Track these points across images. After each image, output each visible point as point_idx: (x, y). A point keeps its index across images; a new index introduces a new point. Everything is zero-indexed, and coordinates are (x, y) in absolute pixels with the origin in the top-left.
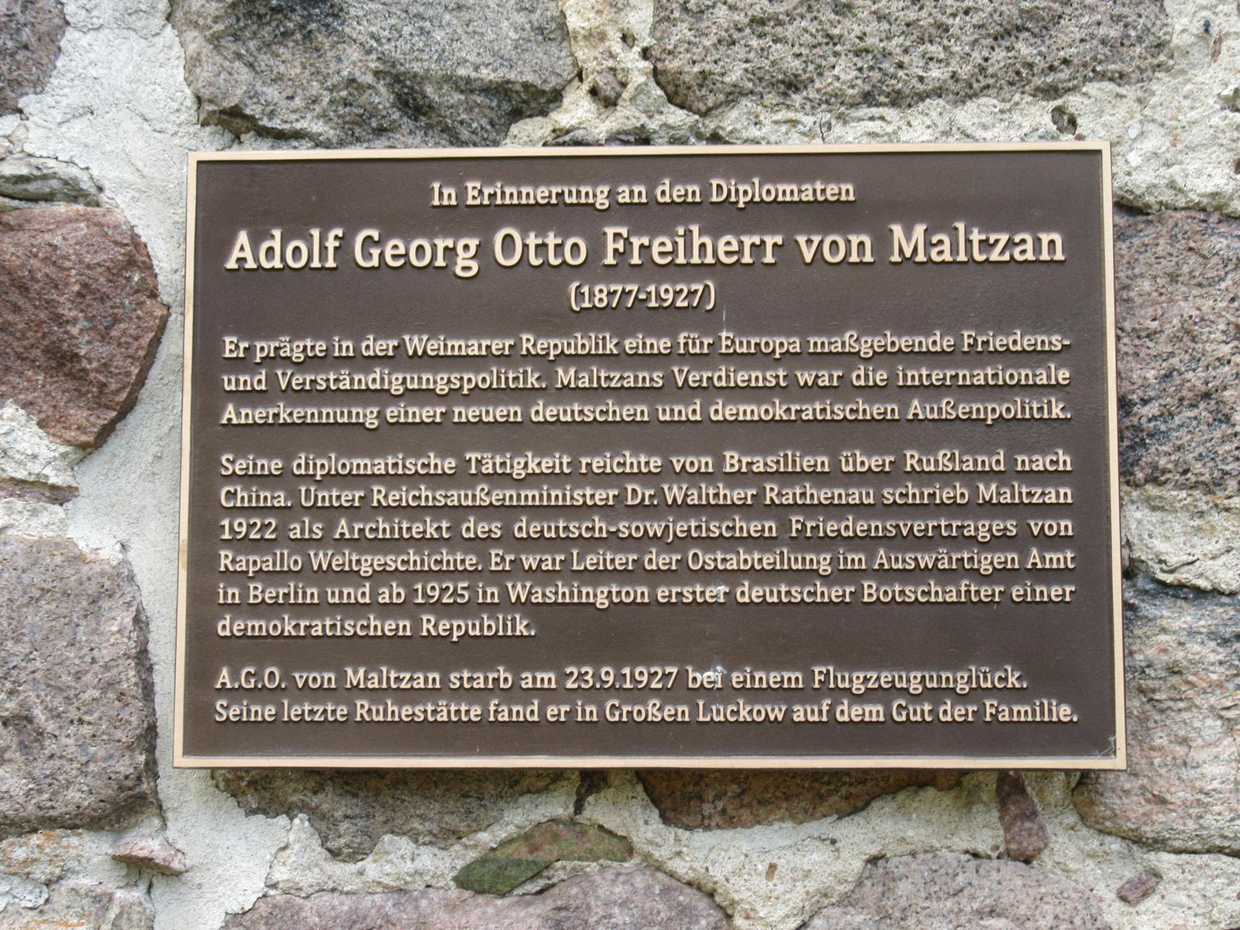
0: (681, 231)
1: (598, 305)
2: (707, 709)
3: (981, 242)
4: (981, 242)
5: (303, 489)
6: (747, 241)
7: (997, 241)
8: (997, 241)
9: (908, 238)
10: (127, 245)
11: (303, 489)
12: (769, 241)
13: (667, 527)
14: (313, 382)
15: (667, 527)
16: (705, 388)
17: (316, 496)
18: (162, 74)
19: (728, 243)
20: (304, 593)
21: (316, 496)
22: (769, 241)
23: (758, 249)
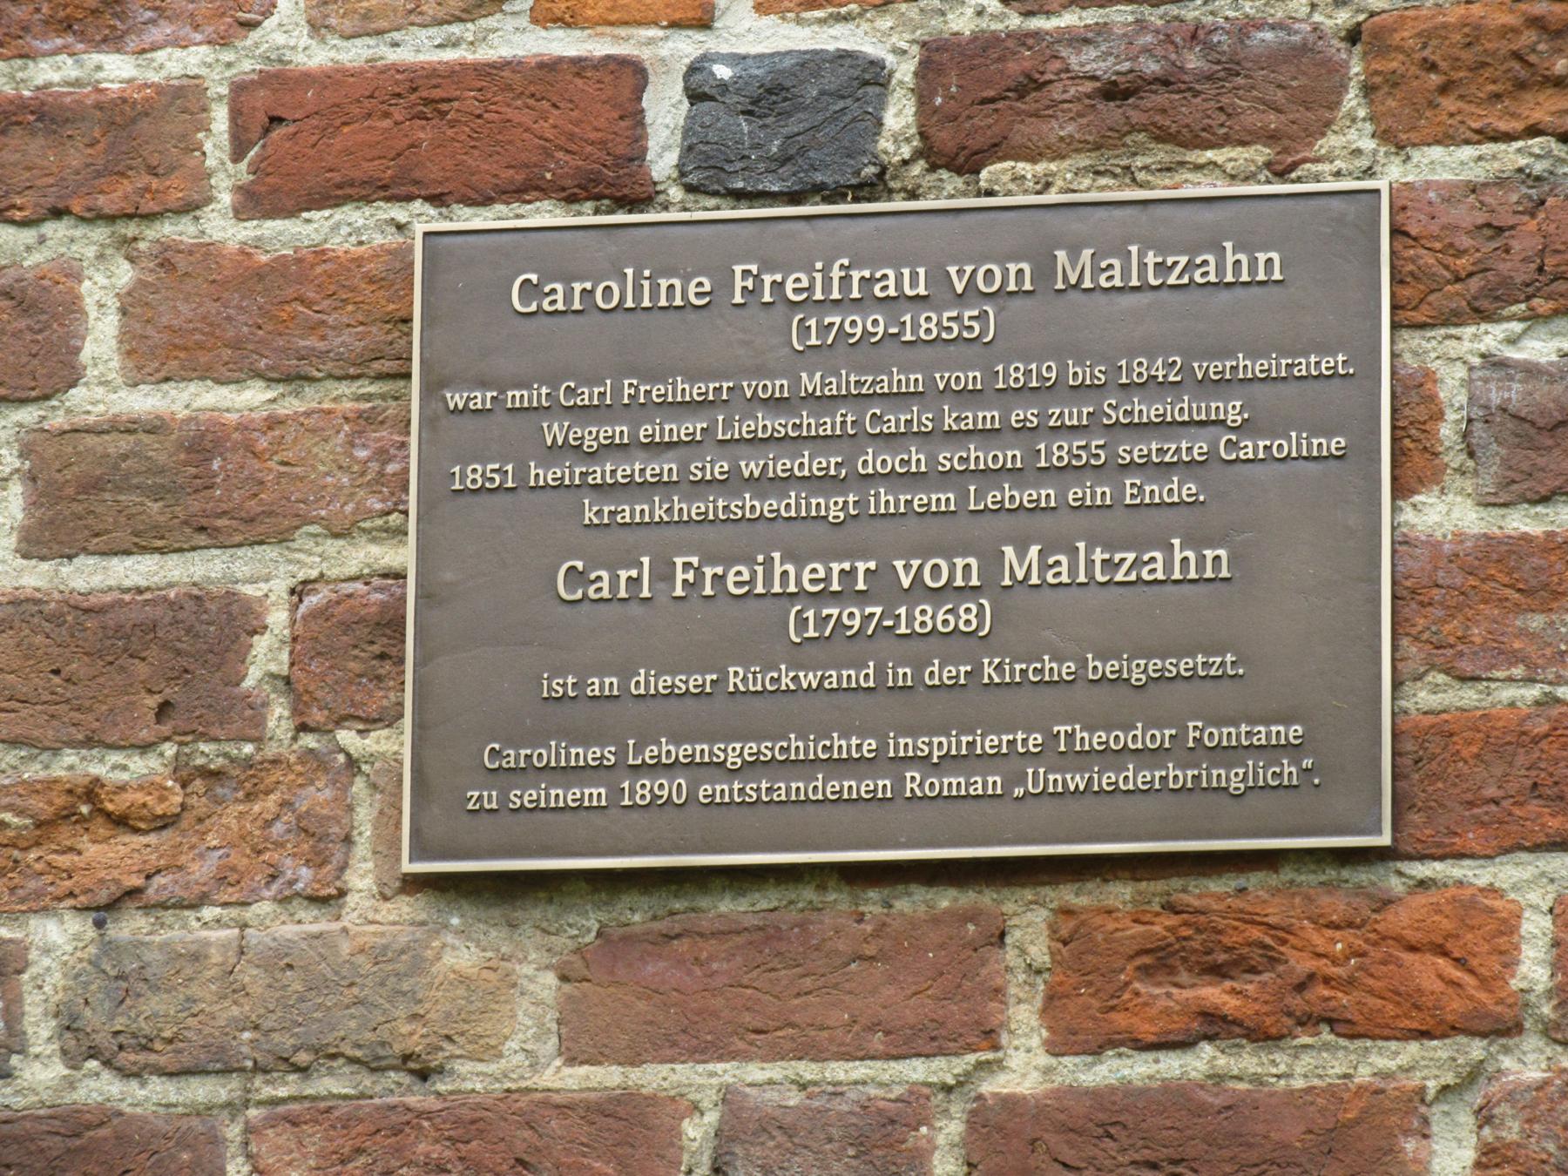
0: (760, 558)
1: (918, 629)
2: (728, 424)
3: (1156, 264)
4: (1156, 264)
5: (1030, 771)
6: (1005, 738)
7: (1175, 263)
8: (1175, 263)
9: (1021, 560)
10: (1141, 169)
11: (1030, 771)
12: (861, 567)
13: (766, 465)
14: (1011, 743)
15: (766, 465)
16: (711, 402)
17: (1046, 781)
18: (1459, 1153)
19: (798, 280)
20: (808, 505)
21: (1046, 781)
22: (861, 567)
23: (718, 390)
